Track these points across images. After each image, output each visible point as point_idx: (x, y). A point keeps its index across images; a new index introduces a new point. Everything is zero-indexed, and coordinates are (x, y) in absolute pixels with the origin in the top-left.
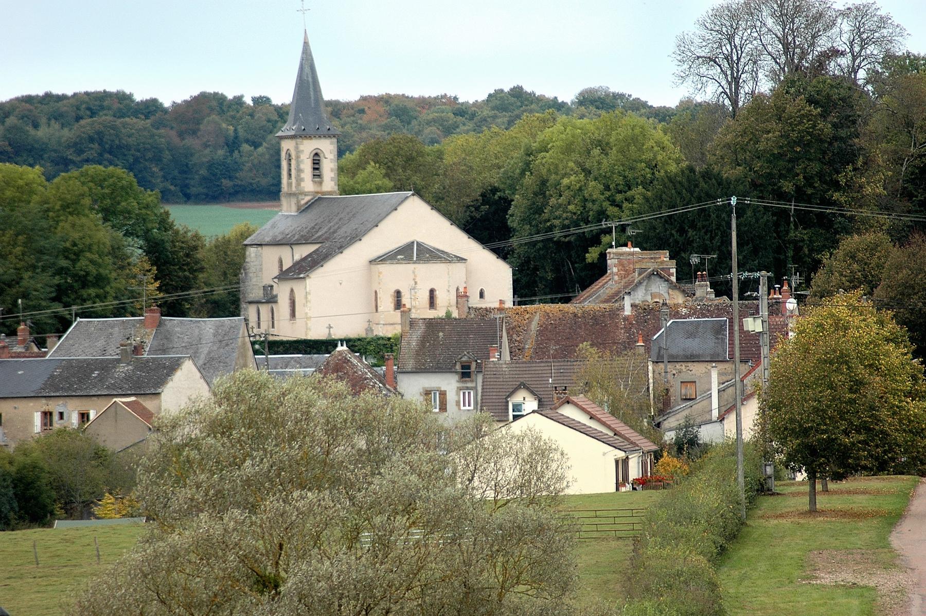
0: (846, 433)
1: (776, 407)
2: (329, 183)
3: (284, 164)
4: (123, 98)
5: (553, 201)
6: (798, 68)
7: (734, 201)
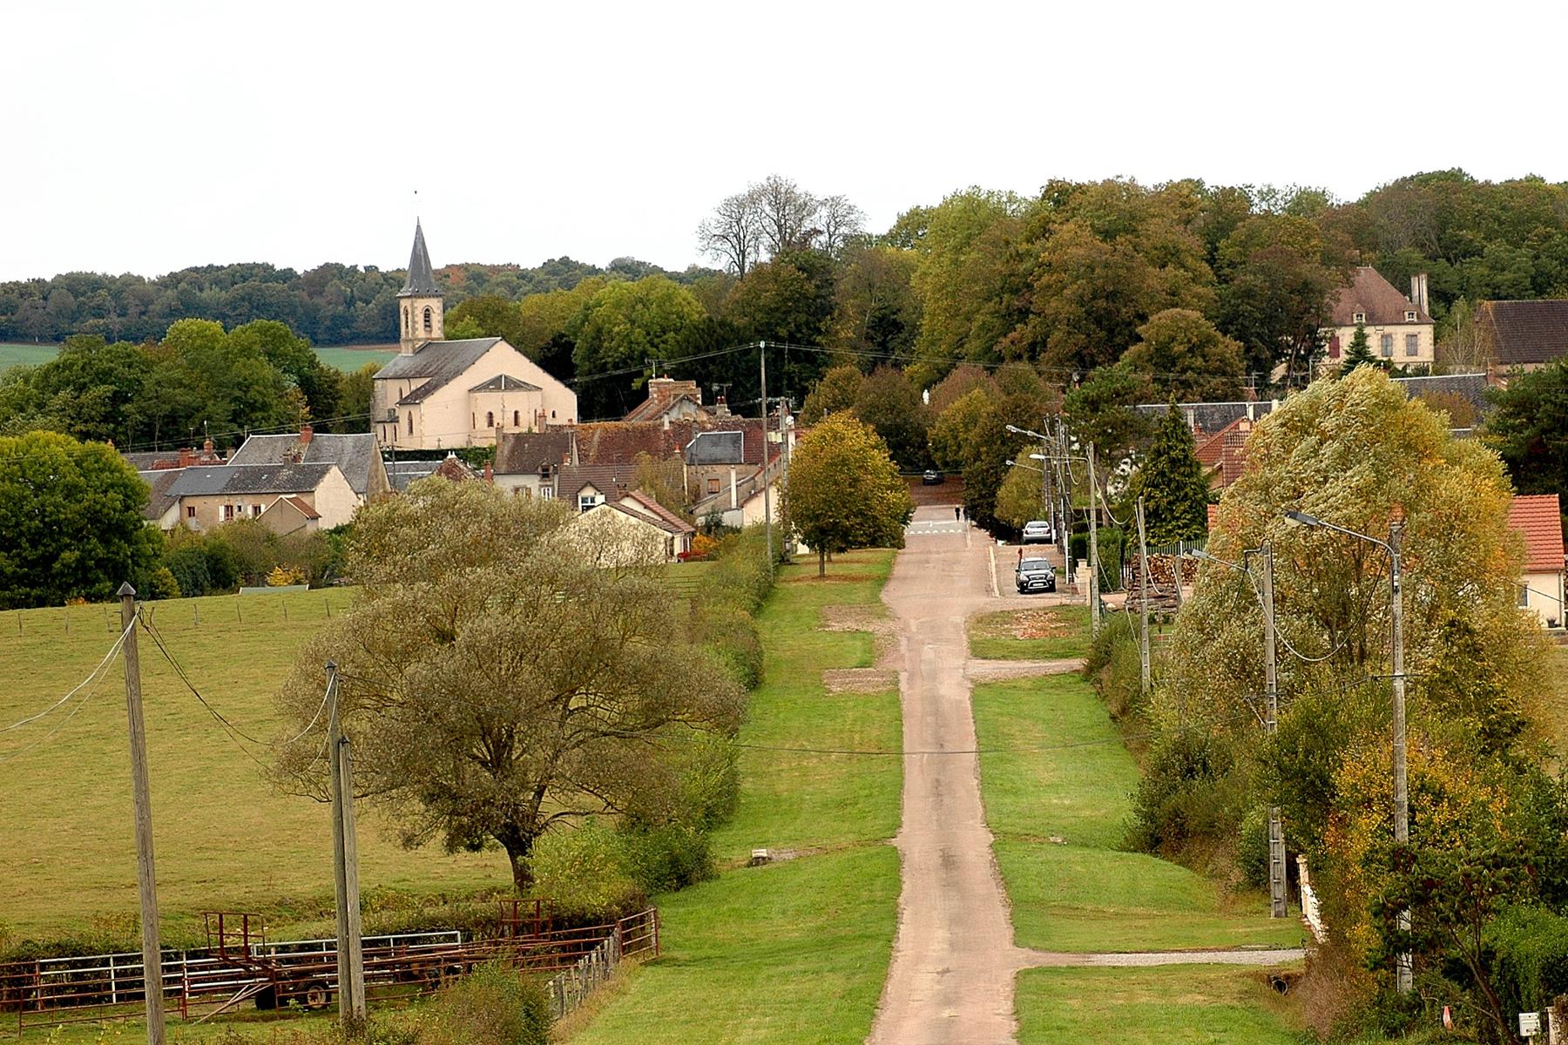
0: (847, 518)
1: (796, 498)
2: (437, 332)
3: (403, 317)
4: (267, 268)
5: (606, 344)
6: (789, 243)
7: (762, 345)
